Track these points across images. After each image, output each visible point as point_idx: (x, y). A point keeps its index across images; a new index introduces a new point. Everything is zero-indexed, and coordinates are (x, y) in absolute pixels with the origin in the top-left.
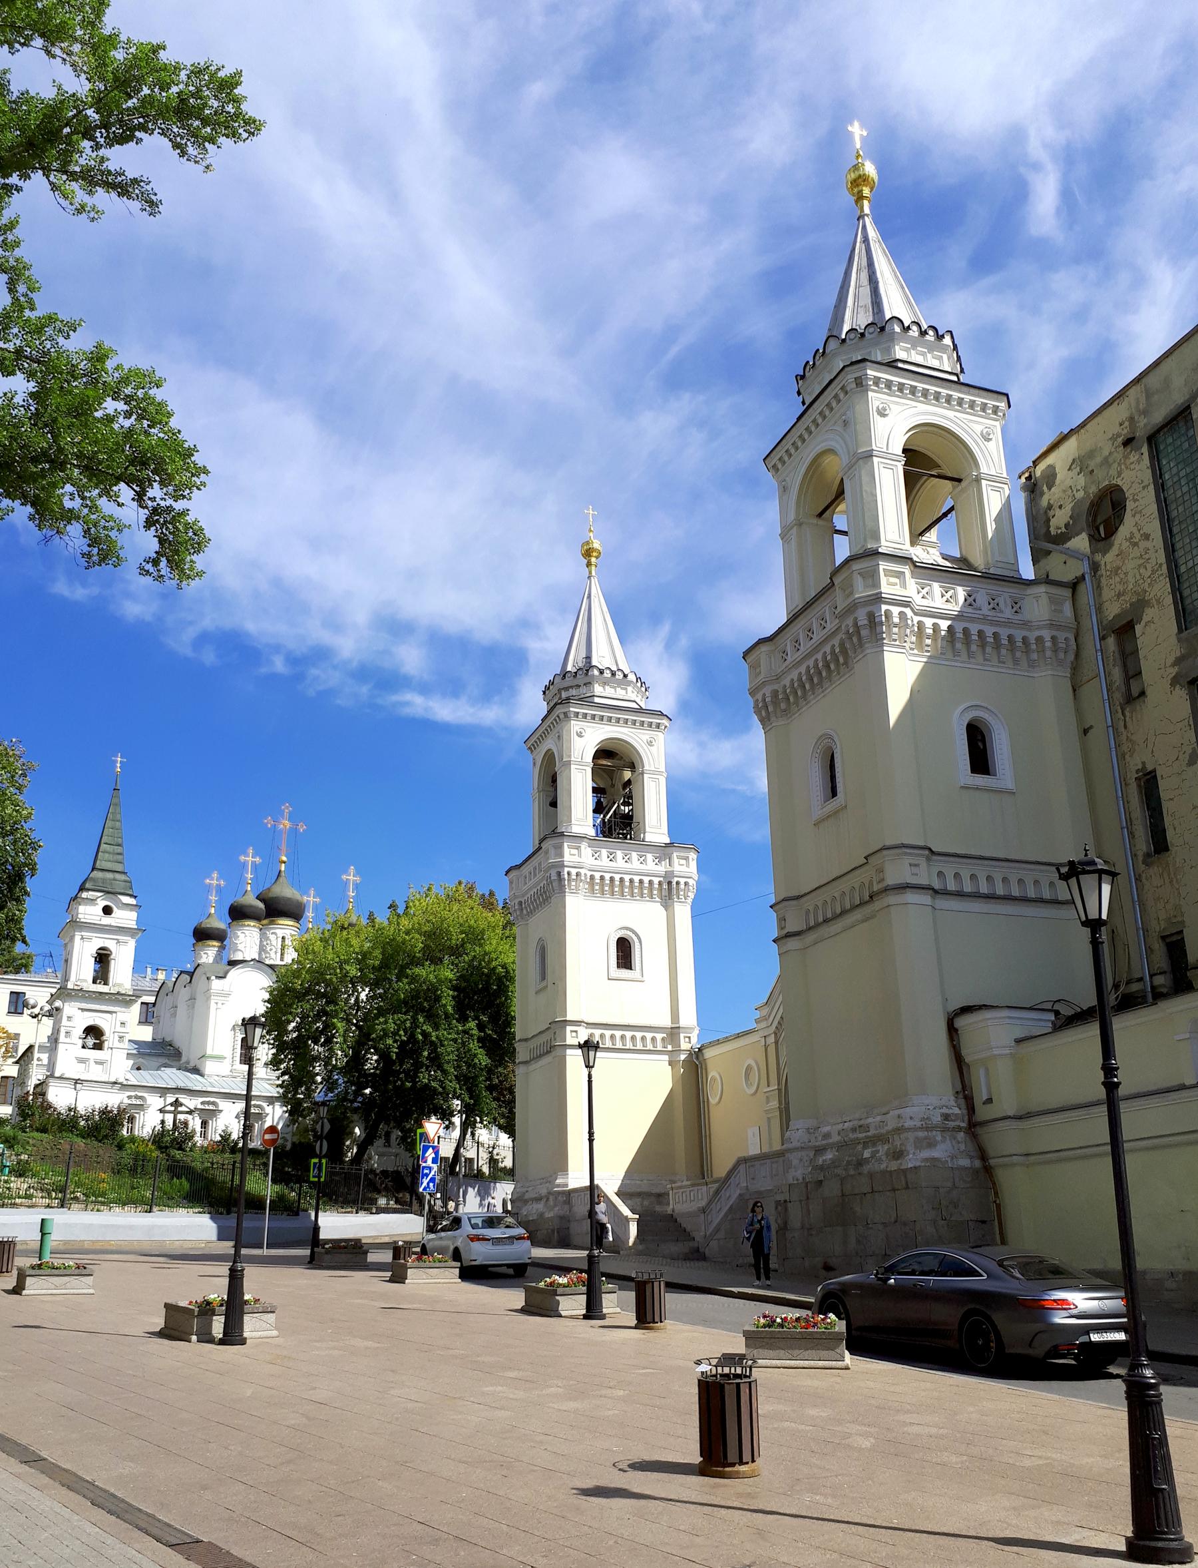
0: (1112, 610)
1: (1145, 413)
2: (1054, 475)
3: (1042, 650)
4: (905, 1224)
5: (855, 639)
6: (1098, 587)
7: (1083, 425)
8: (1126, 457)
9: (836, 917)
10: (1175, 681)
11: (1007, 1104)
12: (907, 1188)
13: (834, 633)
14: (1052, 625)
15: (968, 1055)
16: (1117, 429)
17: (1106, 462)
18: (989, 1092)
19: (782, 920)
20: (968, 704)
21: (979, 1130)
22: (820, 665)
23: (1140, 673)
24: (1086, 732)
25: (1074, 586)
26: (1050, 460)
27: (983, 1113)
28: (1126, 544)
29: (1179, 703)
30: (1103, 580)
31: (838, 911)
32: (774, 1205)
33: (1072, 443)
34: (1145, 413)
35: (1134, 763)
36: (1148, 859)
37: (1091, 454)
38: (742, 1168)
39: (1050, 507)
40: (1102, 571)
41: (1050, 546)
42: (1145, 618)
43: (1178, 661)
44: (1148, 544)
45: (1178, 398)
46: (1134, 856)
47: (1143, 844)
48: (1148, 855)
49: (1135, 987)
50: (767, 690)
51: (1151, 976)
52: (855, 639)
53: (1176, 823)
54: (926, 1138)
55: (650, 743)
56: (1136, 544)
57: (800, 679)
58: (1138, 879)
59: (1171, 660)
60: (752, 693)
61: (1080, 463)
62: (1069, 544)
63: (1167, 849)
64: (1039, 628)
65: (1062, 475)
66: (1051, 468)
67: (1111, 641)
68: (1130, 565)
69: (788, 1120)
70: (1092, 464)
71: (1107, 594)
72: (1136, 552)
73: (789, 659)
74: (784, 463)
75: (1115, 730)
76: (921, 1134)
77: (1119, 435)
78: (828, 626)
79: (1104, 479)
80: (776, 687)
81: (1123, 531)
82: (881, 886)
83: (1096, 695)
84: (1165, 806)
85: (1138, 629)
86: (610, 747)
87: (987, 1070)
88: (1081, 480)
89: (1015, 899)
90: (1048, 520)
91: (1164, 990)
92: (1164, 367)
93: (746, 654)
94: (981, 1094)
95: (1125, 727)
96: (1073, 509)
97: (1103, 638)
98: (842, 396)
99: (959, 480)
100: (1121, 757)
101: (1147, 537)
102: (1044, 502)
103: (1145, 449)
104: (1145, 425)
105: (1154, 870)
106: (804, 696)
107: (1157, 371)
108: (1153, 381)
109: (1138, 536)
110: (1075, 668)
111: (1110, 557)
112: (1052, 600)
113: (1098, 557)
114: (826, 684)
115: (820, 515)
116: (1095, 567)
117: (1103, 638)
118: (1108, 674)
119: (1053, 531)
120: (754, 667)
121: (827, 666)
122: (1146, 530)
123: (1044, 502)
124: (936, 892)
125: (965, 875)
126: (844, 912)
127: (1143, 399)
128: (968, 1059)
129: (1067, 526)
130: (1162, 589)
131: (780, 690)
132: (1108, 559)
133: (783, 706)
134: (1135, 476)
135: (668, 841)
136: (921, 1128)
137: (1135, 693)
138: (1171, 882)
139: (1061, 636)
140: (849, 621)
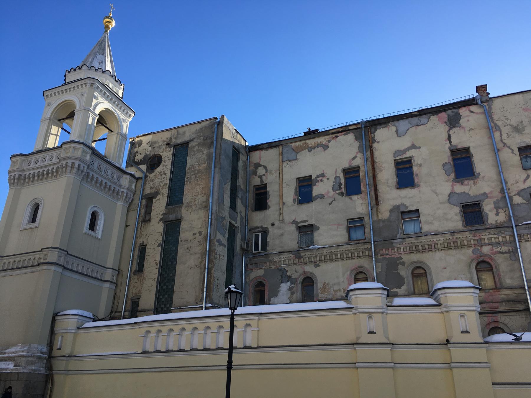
0: (148, 191)
1: (175, 138)
2: (141, 144)
3: (122, 196)
5: (64, 169)
6: (145, 183)
7: (155, 133)
9: (18, 268)
10: (161, 220)
11: (67, 351)
12: (18, 380)
14: (128, 189)
15: (57, 329)
16: (165, 139)
17: (159, 147)
20: (92, 206)
22: (45, 173)
24: (127, 226)
25: (138, 179)
27: (55, 353)
29: (160, 227)
30: (147, 182)
34: (175, 138)
35: (140, 241)
37: (155, 143)
39: (137, 152)
40: (148, 179)
41: (133, 164)
42: (157, 198)
43: (164, 214)
44: (165, 177)
45: (186, 138)
48: (135, 271)
50: (17, 173)
51: (124, 311)
52: (64, 169)
53: (148, 264)
54: (32, 361)
56: (161, 175)
59: (162, 213)
60: (10, 172)
61: (151, 144)
62: (139, 166)
63: (142, 271)
64: (124, 189)
66: (141, 141)
67: (144, 201)
68: (158, 180)
71: (147, 186)
72: (161, 177)
73: (39, 164)
74: (55, 95)
77: (165, 141)
80: (21, 173)
81: (159, 169)
87: (63, 337)
89: (89, 276)
96: (144, 156)
97: (142, 199)
99: (112, 132)
100: (136, 238)
101: (165, 174)
102: (136, 150)
103: (172, 149)
106: (42, 179)
108: (181, 131)
109: (162, 173)
110: (130, 205)
113: (148, 174)
116: (146, 176)
119: (136, 160)
120: (13, 163)
122: (166, 172)
124: (65, 268)
126: (22, 267)
129: (141, 160)
130: (165, 191)
131: (23, 176)
132: (151, 176)
134: (167, 155)
136: (32, 357)
137: (147, 218)
138: (141, 282)
139: (130, 193)
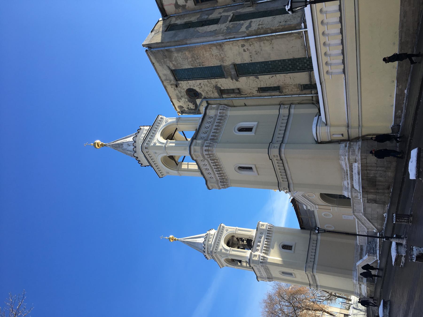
0: (216, 95)
1: (170, 81)
2: (181, 106)
3: (223, 113)
5: (211, 156)
6: (210, 98)
7: (170, 97)
8: (180, 87)
10: (237, 80)
11: (344, 130)
16: (173, 89)
17: (180, 92)
18: (339, 135)
19: (284, 189)
22: (216, 167)
24: (245, 105)
25: (208, 104)
26: (177, 107)
29: (243, 80)
31: (284, 171)
32: (368, 204)
33: (173, 100)
34: (170, 81)
35: (256, 93)
37: (177, 96)
38: (356, 214)
39: (188, 108)
41: (197, 109)
42: (220, 86)
43: (232, 79)
45: (168, 72)
48: (280, 92)
50: (220, 184)
51: (312, 94)
52: (211, 156)
54: (352, 152)
55: (227, 231)
56: (201, 87)
57: (219, 174)
59: (231, 81)
60: (220, 189)
64: (217, 113)
65: (181, 104)
67: (224, 96)
69: (342, 197)
70: (180, 96)
71: (212, 96)
72: (203, 87)
74: (160, 170)
76: (351, 153)
78: (206, 163)
79: (184, 93)
81: (198, 89)
82: (279, 156)
85: (222, 88)
86: (226, 242)
88: (183, 99)
90: (191, 109)
91: (316, 91)
92: (161, 75)
94: (340, 137)
95: (246, 94)
97: (223, 98)
98: (149, 153)
99: (177, 129)
100: (253, 96)
101: (200, 84)
102: (186, 109)
103: (179, 82)
104: (174, 82)
105: (284, 91)
108: (163, 78)
109: (199, 86)
111: (203, 94)
113: (203, 97)
114: (221, 167)
115: (177, 165)
116: (205, 98)
118: (232, 98)
119: (194, 108)
121: (216, 165)
122: (198, 84)
123: (186, 109)
124: (282, 142)
126: (285, 170)
127: (167, 81)
129: (193, 104)
133: (225, 180)
134: (185, 85)
135: (256, 230)
137: (237, 91)
139: (220, 108)
140: (206, 156)
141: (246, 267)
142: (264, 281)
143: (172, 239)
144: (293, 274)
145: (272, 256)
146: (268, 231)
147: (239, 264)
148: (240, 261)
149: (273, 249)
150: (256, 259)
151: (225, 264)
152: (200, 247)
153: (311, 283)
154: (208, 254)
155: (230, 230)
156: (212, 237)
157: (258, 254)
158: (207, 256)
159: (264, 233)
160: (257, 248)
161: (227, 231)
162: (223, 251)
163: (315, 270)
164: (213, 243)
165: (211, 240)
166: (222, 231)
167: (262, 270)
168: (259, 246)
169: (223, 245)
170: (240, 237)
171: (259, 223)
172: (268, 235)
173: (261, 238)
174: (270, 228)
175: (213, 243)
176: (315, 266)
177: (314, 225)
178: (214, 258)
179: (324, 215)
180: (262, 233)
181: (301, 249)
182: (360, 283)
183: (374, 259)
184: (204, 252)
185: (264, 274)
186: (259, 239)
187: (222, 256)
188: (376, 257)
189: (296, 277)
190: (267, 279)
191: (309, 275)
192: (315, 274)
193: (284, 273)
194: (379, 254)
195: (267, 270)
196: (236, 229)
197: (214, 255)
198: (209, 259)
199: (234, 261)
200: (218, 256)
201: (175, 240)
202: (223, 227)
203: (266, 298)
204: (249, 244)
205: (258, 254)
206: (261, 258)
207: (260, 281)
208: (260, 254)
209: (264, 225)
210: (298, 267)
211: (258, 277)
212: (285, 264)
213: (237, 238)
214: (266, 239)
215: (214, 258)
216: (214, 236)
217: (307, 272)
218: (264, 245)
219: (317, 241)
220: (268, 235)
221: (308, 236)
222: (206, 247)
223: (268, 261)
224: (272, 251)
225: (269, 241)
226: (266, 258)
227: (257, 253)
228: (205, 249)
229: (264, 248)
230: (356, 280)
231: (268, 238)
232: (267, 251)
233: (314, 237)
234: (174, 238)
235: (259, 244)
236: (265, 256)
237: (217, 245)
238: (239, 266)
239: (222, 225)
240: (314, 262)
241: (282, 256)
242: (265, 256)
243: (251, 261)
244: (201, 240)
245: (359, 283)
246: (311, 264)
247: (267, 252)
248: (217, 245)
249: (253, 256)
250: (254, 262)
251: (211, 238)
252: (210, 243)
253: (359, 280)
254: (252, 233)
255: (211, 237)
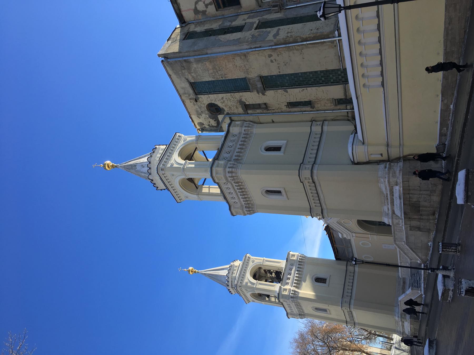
0: (241, 110)
1: (189, 95)
2: (201, 123)
4: (421, 184)
5: (235, 178)
6: (234, 114)
7: (189, 113)
8: (200, 102)
10: (263, 94)
11: (383, 150)
13: (232, 184)
14: (242, 127)
16: (192, 103)
17: (200, 107)
18: (378, 154)
21: (391, 159)
23: (259, 104)
24: (273, 122)
25: (232, 120)
27: (385, 157)
28: (223, 104)
30: (233, 112)
31: (317, 195)
32: (411, 231)
33: (193, 117)
34: (189, 95)
35: (284, 108)
36: (313, 107)
37: (197, 111)
38: (397, 243)
39: (209, 125)
42: (245, 101)
44: (225, 98)
45: (187, 85)
46: (311, 111)
47: (308, 108)
49: (350, 115)
50: (245, 210)
51: (347, 109)
52: (235, 178)
54: (392, 174)
55: (253, 262)
56: (224, 101)
58: (318, 111)
60: (245, 215)
61: (199, 115)
62: (220, 121)
63: (310, 101)
65: (201, 121)
67: (249, 112)
69: (382, 224)
71: (236, 111)
72: (226, 101)
74: (178, 194)
75: (274, 113)
76: (391, 175)
80: (244, 207)
83: (263, 118)
84: (298, 101)
86: (252, 274)
88: (204, 115)
91: (352, 106)
93: (232, 214)
94: (379, 157)
97: (248, 114)
99: (196, 148)
100: (282, 112)
101: (223, 98)
102: (207, 127)
103: (199, 96)
104: (193, 96)
105: (316, 106)
107: (179, 91)
108: (181, 91)
109: (222, 101)
110: (255, 123)
112: (235, 126)
113: (225, 113)
115: (197, 188)
116: (228, 114)
117: (248, 114)
119: (216, 125)
120: (237, 213)
123: (207, 127)
125: (311, 156)
127: (186, 95)
128: (368, 160)
129: (215, 121)
132: (226, 110)
133: (250, 205)
134: (206, 99)
137: (264, 106)
139: (245, 125)
140: (229, 179)
141: (275, 302)
142: (295, 318)
143: (192, 271)
144: (328, 310)
145: (304, 290)
146: (299, 262)
147: (267, 299)
148: (268, 296)
149: (305, 282)
150: (286, 293)
151: (251, 299)
152: (224, 280)
153: (348, 320)
154: (232, 288)
155: (256, 260)
156: (236, 269)
157: (289, 287)
158: (231, 290)
159: (295, 264)
160: (287, 281)
161: (253, 262)
162: (249, 284)
163: (352, 306)
164: (237, 276)
165: (235, 272)
166: (248, 263)
167: (293, 305)
168: (289, 279)
169: (249, 278)
170: (267, 268)
171: (289, 254)
172: (300, 266)
173: (291, 269)
174: (301, 259)
175: (237, 276)
176: (352, 301)
177: (351, 255)
178: (238, 293)
179: (362, 244)
180: (292, 265)
181: (336, 282)
182: (403, 320)
183: (418, 293)
184: (228, 286)
185: (295, 310)
186: (290, 271)
187: (249, 290)
188: (421, 291)
189: (330, 314)
190: (298, 316)
191: (346, 311)
192: (352, 310)
193: (317, 309)
194: (424, 288)
195: (298, 306)
196: (264, 259)
197: (239, 289)
198: (234, 293)
199: (262, 296)
200: (244, 290)
201: (195, 272)
202: (249, 258)
203: (297, 337)
204: (278, 277)
205: (289, 287)
206: (292, 292)
207: (291, 319)
208: (290, 287)
209: (295, 255)
210: (333, 303)
211: (289, 314)
212: (319, 298)
213: (265, 270)
214: (297, 271)
215: (238, 293)
216: (238, 268)
217: (344, 308)
218: (295, 278)
219: (354, 273)
220: (300, 266)
221: (344, 267)
222: (230, 280)
223: (300, 295)
224: (304, 284)
225: (300, 273)
226: (297, 292)
227: (287, 287)
228: (228, 282)
229: (295, 281)
230: (398, 317)
231: (299, 270)
232: (298, 285)
233: (351, 268)
234: (194, 270)
235: (289, 276)
236: (296, 290)
237: (243, 278)
238: (267, 301)
239: (248, 255)
240: (351, 296)
241: (315, 290)
242: (296, 290)
243: (280, 296)
244: (224, 273)
245: (401, 321)
246: (348, 299)
247: (298, 286)
248: (243, 278)
249: (282, 290)
250: (284, 296)
251: (235, 270)
252: (234, 275)
253: (401, 317)
254: (281, 264)
255: (235, 268)
